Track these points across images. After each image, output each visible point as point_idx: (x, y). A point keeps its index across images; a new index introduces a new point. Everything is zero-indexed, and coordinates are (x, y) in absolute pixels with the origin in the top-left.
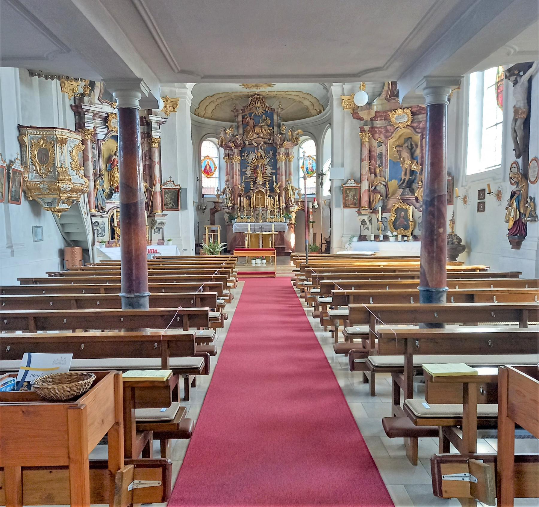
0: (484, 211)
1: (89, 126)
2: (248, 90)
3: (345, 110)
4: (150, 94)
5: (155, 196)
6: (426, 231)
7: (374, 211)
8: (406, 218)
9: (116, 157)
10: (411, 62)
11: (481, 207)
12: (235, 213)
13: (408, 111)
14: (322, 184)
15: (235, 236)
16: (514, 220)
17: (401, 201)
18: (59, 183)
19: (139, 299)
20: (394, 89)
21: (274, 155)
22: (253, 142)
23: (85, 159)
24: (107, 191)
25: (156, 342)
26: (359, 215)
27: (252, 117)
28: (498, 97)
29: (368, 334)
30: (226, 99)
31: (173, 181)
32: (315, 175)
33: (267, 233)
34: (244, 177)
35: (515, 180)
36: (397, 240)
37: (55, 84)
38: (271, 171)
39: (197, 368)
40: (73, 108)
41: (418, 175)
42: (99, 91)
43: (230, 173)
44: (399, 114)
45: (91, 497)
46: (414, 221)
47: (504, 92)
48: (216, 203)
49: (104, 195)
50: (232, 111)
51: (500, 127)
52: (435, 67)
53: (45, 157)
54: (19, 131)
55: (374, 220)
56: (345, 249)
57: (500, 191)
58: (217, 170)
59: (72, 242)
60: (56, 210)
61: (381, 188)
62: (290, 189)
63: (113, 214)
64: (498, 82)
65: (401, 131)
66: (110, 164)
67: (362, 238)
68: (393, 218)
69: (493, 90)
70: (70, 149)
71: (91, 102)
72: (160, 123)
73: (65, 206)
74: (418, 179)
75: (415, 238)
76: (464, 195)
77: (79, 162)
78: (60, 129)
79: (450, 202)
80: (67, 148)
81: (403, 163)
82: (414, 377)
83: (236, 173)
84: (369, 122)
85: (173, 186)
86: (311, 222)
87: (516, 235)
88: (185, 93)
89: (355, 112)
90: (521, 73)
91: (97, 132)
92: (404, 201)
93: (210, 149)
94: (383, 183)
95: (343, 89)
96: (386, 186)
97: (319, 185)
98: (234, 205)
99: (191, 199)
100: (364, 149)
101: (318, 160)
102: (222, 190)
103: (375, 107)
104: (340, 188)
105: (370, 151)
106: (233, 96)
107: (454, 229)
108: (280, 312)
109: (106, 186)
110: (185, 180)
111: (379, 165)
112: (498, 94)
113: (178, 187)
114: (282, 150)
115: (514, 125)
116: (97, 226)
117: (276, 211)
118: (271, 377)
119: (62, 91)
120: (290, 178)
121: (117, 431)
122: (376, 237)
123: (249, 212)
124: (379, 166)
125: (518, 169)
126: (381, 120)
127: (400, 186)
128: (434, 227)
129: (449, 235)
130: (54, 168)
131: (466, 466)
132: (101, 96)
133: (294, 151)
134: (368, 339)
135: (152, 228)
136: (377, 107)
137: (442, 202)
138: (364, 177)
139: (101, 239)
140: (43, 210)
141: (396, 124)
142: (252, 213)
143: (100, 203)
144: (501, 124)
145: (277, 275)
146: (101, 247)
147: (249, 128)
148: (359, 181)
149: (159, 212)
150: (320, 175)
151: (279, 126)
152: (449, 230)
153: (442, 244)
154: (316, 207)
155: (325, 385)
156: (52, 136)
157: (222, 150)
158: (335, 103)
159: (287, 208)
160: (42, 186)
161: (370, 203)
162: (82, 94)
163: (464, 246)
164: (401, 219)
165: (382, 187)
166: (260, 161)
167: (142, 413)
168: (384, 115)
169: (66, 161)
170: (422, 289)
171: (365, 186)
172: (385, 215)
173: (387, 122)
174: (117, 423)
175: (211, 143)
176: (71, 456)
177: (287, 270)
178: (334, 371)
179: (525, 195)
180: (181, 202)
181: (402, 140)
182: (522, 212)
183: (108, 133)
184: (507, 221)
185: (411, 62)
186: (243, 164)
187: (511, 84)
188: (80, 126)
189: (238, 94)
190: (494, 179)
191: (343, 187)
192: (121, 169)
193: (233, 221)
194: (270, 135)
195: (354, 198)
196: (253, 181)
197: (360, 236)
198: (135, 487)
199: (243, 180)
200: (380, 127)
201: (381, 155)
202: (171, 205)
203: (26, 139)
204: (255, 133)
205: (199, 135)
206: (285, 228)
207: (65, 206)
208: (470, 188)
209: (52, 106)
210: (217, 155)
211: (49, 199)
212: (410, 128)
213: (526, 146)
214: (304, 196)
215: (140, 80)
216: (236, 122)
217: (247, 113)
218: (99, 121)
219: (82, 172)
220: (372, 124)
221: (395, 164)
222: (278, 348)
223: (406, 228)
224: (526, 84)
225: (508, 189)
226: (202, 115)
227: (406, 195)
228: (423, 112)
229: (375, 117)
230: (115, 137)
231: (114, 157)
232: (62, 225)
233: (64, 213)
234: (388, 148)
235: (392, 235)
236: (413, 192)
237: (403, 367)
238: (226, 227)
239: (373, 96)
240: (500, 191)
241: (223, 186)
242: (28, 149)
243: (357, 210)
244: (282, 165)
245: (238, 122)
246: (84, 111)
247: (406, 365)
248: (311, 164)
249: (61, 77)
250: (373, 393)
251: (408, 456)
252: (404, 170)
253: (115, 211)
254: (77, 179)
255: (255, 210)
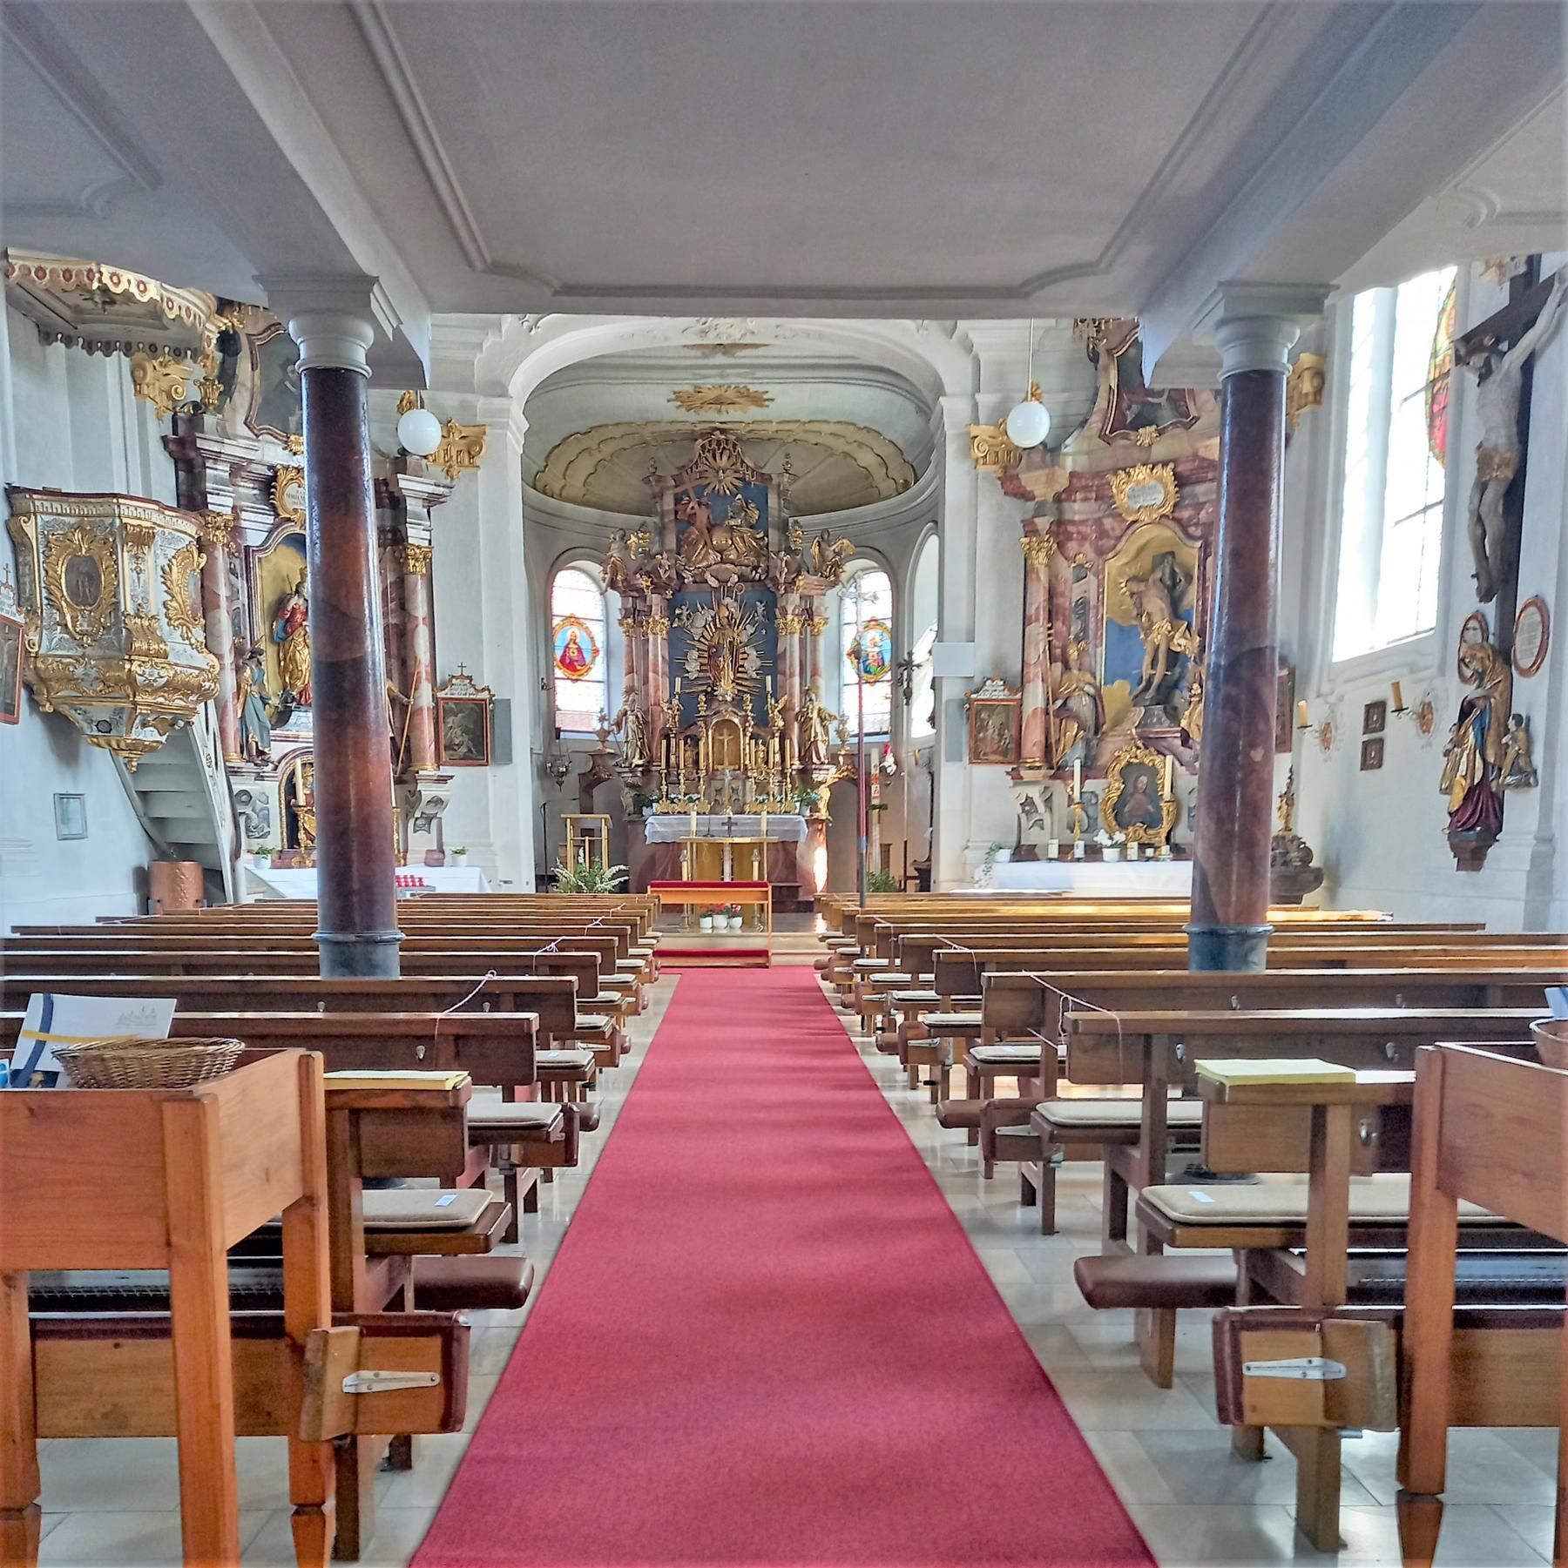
0: (1380, 765)
1: (221, 503)
2: (692, 416)
3: (981, 469)
4: (397, 332)
5: (416, 720)
6: (1213, 759)
7: (1059, 772)
8: (1153, 794)
9: (301, 601)
10: (1180, 245)
11: (1372, 755)
12: (654, 786)
13: (1167, 473)
14: (908, 694)
15: (653, 857)
16: (1465, 784)
17: (1139, 743)
18: (131, 661)
19: (370, 948)
20: (1125, 405)
21: (770, 616)
22: (708, 576)
23: (207, 602)
24: (275, 701)
25: (419, 1039)
26: (1015, 785)
27: (704, 500)
28: (1431, 427)
29: (1037, 1062)
30: (627, 442)
31: (470, 678)
32: (888, 676)
33: (747, 840)
34: (678, 680)
35: (1474, 665)
36: (1124, 857)
37: (114, 367)
38: (759, 663)
39: (540, 1127)
40: (172, 446)
41: (1191, 665)
42: (248, 399)
43: (637, 667)
44: (1138, 482)
45: (239, 1416)
46: (1175, 800)
47: (1450, 411)
48: (595, 756)
49: (266, 714)
50: (646, 480)
51: (1437, 516)
52: (1250, 256)
53: (89, 583)
54: (11, 505)
55: (1060, 799)
56: (973, 882)
57: (1429, 704)
58: (600, 659)
59: (171, 845)
60: (123, 745)
61: (1082, 705)
62: (815, 715)
63: (293, 773)
64: (1434, 382)
65: (1145, 534)
66: (281, 622)
67: (1024, 853)
68: (1115, 795)
69: (1420, 405)
70: (163, 562)
71: (224, 429)
72: (432, 501)
73: (150, 735)
74: (1189, 676)
75: (1179, 852)
76: (1324, 722)
77: (189, 602)
78: (132, 498)
79: (1284, 744)
80: (154, 558)
81: (1148, 630)
82: (1170, 1156)
83: (656, 665)
84: (1051, 507)
85: (469, 693)
86: (874, 807)
87: (1472, 828)
88: (506, 412)
89: (1010, 469)
90: (1504, 346)
91: (244, 524)
92: (1148, 741)
93: (579, 595)
94: (1087, 688)
95: (975, 406)
96: (1097, 699)
97: (903, 694)
98: (650, 762)
99: (523, 736)
100: (1032, 588)
101: (899, 630)
102: (614, 717)
103: (1069, 460)
104: (962, 703)
105: (1051, 594)
106: (647, 434)
107: (1292, 819)
108: (778, 1045)
109: (272, 687)
110: (506, 675)
111: (1076, 637)
112: (1432, 416)
113: (485, 695)
114: (793, 601)
115: (1476, 501)
116: (246, 803)
117: (774, 780)
118: (752, 1190)
119: (138, 392)
120: (814, 683)
121: (311, 1223)
122: (1065, 851)
123: (693, 783)
124: (1078, 640)
125: (1485, 631)
126: (1086, 499)
127: (1137, 700)
128: (1236, 743)
129: (1276, 838)
130: (117, 617)
131: (1313, 1338)
132: (254, 413)
133: (827, 602)
134: (1037, 1076)
135: (407, 816)
136: (1074, 461)
137: (1262, 668)
138: (1032, 670)
139: (256, 844)
140: (85, 747)
141: (1130, 511)
142: (702, 788)
143: (254, 737)
144: (1440, 508)
145: (774, 960)
146: (257, 864)
147: (694, 533)
148: (1018, 684)
149: (429, 769)
150: (903, 667)
151: (784, 527)
152: (1276, 825)
153: (1260, 795)
154: (892, 769)
155: (911, 1208)
156: (108, 521)
157: (615, 597)
158: (951, 449)
159: (805, 772)
160: (80, 671)
161: (1048, 749)
162: (196, 405)
163: (1319, 869)
164: (1139, 797)
165: (1086, 700)
166: (728, 632)
167: (376, 1205)
168: (1094, 485)
169: (151, 597)
170: (1196, 929)
171: (1035, 697)
172: (1090, 785)
173: (1104, 507)
174: (309, 1200)
175: (583, 577)
176: (174, 1239)
177: (804, 946)
178: (938, 1179)
179: (1502, 712)
180: (493, 741)
181: (1146, 561)
182: (1491, 759)
183: (275, 527)
184: (1447, 791)
185: (1180, 245)
186: (678, 642)
187: (1473, 378)
188: (192, 499)
189: (664, 427)
190: (1413, 669)
191: (969, 701)
192: (315, 638)
193: (646, 811)
194: (758, 556)
195: (1001, 735)
196: (706, 693)
197: (1019, 846)
198: (364, 1389)
199: (678, 689)
200: (1082, 522)
201: (1083, 604)
202: (463, 750)
203: (30, 529)
204: (714, 549)
205: (548, 553)
206: (798, 832)
207: (150, 735)
208: (1341, 699)
209: (106, 434)
210: (599, 614)
211: (102, 711)
212: (1171, 523)
213: (1510, 565)
214: (856, 740)
215: (365, 283)
216: (656, 514)
217: (688, 486)
218: (248, 490)
219: (198, 634)
220: (1060, 511)
221: (1123, 635)
222: (775, 1126)
223: (1152, 822)
224: (1516, 375)
225: (1453, 693)
226: (557, 491)
227: (1153, 725)
228: (1210, 476)
229: (1070, 491)
230: (298, 542)
231: (294, 601)
232: (144, 795)
233: (147, 759)
234: (1107, 583)
235: (1109, 843)
236: (1173, 715)
237: (1137, 1127)
238: (627, 827)
239: (1064, 427)
240: (1429, 704)
241: (619, 705)
242: (37, 557)
243: (1009, 768)
244: (791, 644)
245: (662, 515)
246: (205, 456)
247: (1148, 1121)
248: (877, 643)
249: (134, 347)
250: (1049, 1228)
251: (1146, 1369)
252: (1149, 648)
253: (299, 762)
254: (185, 653)
255: (712, 776)
